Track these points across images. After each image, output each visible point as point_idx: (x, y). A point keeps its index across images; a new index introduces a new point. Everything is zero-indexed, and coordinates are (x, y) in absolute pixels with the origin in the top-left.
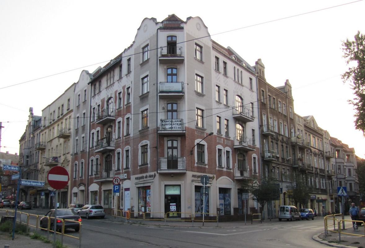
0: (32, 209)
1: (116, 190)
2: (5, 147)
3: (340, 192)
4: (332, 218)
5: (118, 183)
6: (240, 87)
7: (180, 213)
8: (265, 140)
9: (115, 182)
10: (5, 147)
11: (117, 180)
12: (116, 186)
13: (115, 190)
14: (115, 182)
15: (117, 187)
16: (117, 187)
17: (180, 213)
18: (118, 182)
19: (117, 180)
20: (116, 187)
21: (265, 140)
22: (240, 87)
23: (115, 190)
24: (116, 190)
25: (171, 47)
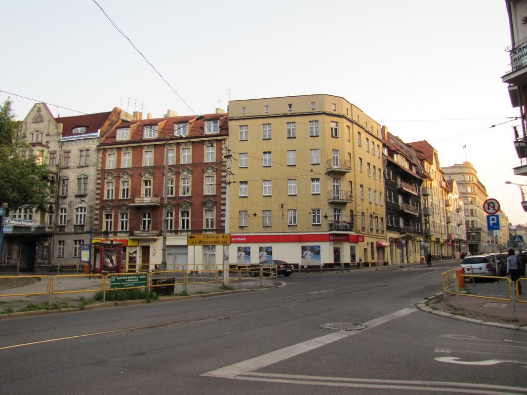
0: (261, 252)
1: (493, 224)
2: (493, 126)
3: (517, 239)
4: (115, 152)
5: (494, 210)
6: (180, 268)
7: (147, 264)
8: (507, 253)
9: (489, 209)
10: (493, 126)
11: (491, 204)
12: (491, 218)
13: (491, 225)
14: (489, 209)
15: (493, 220)
16: (493, 220)
17: (147, 264)
18: (494, 207)
19: (491, 204)
20: (491, 220)
21: (507, 253)
22: (180, 268)
23: (491, 225)
24: (493, 224)
25: (103, 271)
